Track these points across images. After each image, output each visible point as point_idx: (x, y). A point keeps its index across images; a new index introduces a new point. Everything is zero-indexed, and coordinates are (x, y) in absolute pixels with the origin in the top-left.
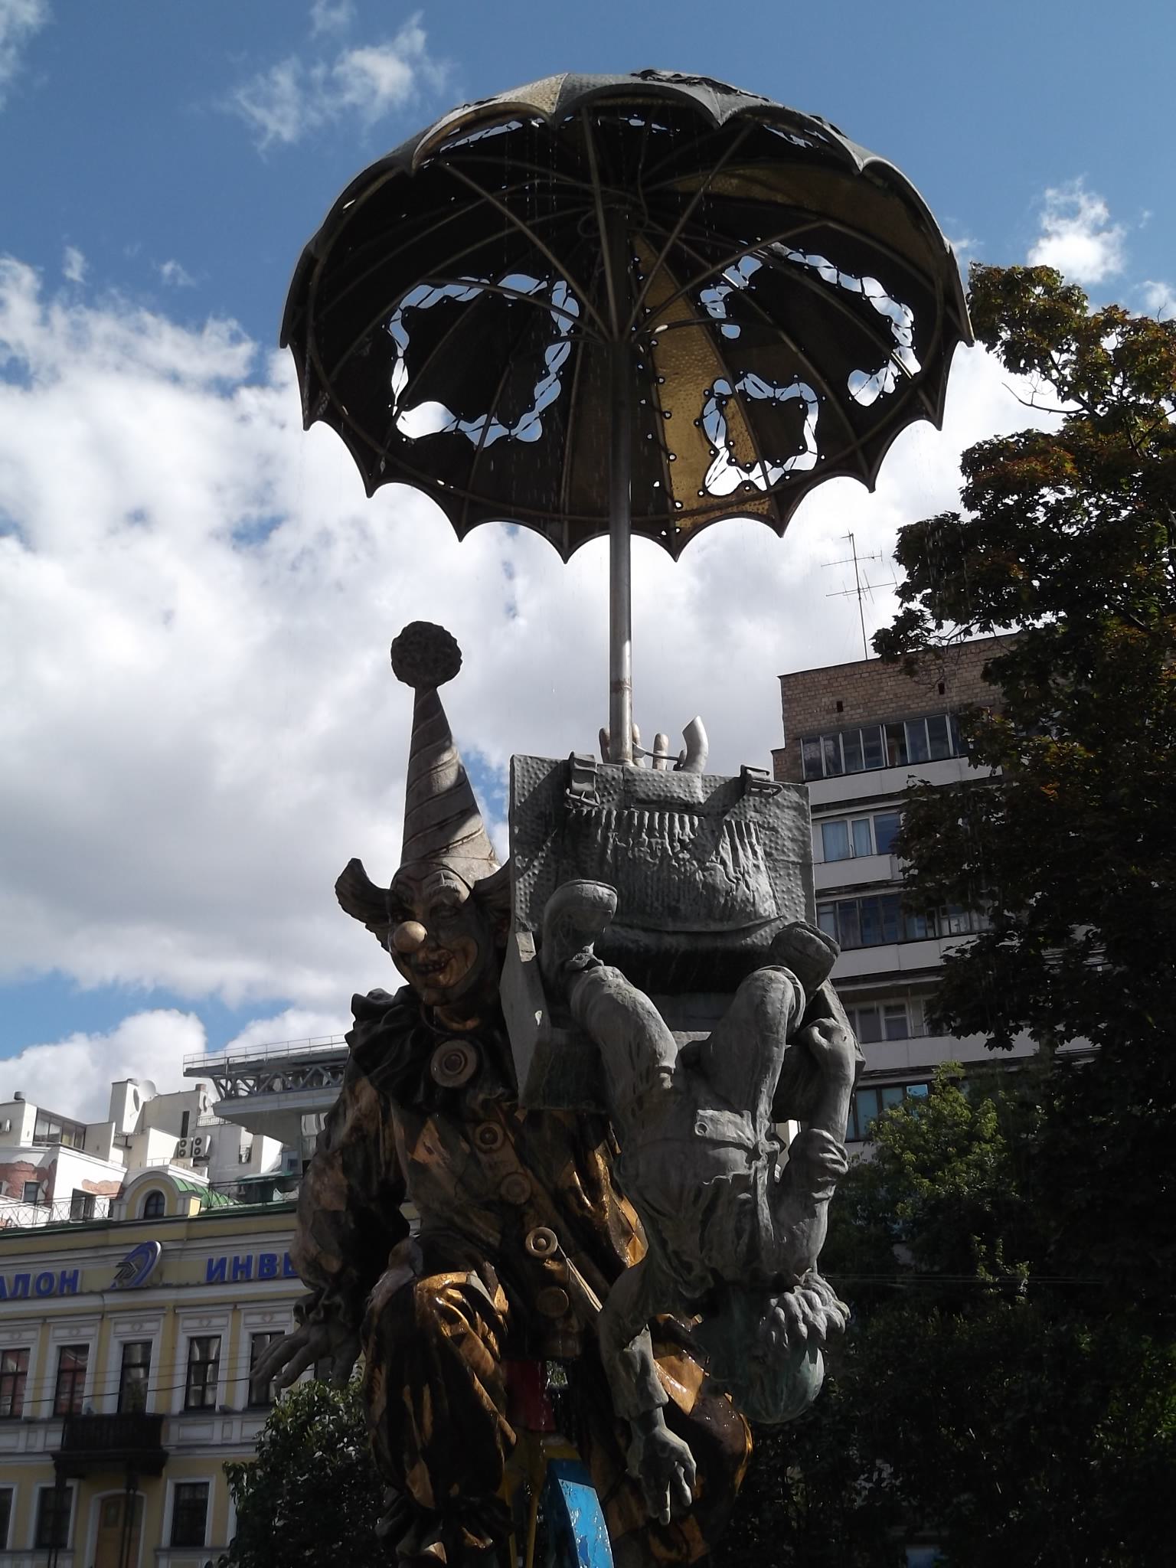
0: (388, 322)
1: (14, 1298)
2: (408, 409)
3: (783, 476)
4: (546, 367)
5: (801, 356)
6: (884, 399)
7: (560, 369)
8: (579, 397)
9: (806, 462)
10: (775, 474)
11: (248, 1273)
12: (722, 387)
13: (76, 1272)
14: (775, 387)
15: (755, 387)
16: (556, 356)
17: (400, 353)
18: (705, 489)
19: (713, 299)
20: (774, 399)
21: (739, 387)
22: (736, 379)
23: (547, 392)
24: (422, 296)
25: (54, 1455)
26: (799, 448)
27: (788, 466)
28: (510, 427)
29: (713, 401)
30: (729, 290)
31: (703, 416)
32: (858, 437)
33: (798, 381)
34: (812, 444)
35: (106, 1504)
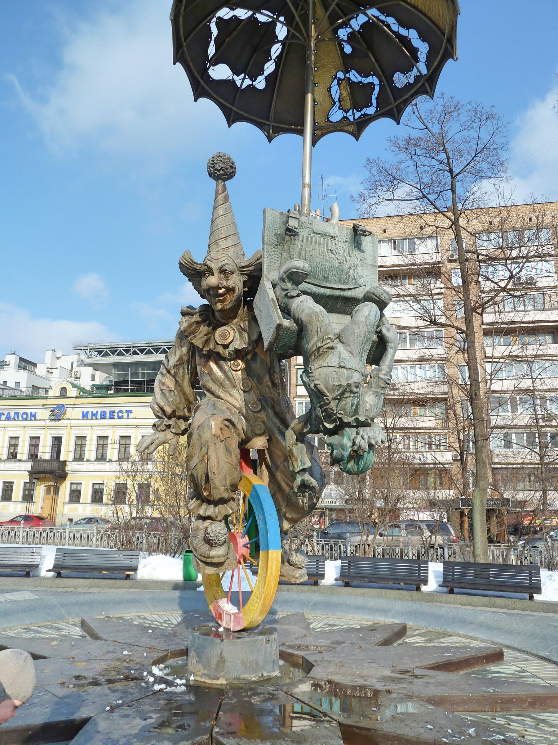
0: (210, 23)
1: (14, 420)
2: (214, 65)
3: (361, 116)
4: (271, 57)
5: (376, 64)
6: (409, 86)
7: (276, 58)
8: (282, 72)
9: (371, 111)
10: (358, 115)
11: (96, 417)
12: (341, 75)
13: (36, 413)
14: (362, 77)
15: (354, 76)
16: (276, 50)
17: (213, 38)
18: (328, 118)
19: (343, 33)
20: (361, 82)
21: (348, 75)
22: (346, 72)
23: (270, 67)
24: (225, 13)
25: (29, 472)
26: (368, 104)
27: (363, 112)
28: (253, 81)
29: (336, 80)
30: (350, 30)
31: (331, 87)
32: (395, 101)
33: (373, 75)
34: (374, 103)
35: (48, 489)
